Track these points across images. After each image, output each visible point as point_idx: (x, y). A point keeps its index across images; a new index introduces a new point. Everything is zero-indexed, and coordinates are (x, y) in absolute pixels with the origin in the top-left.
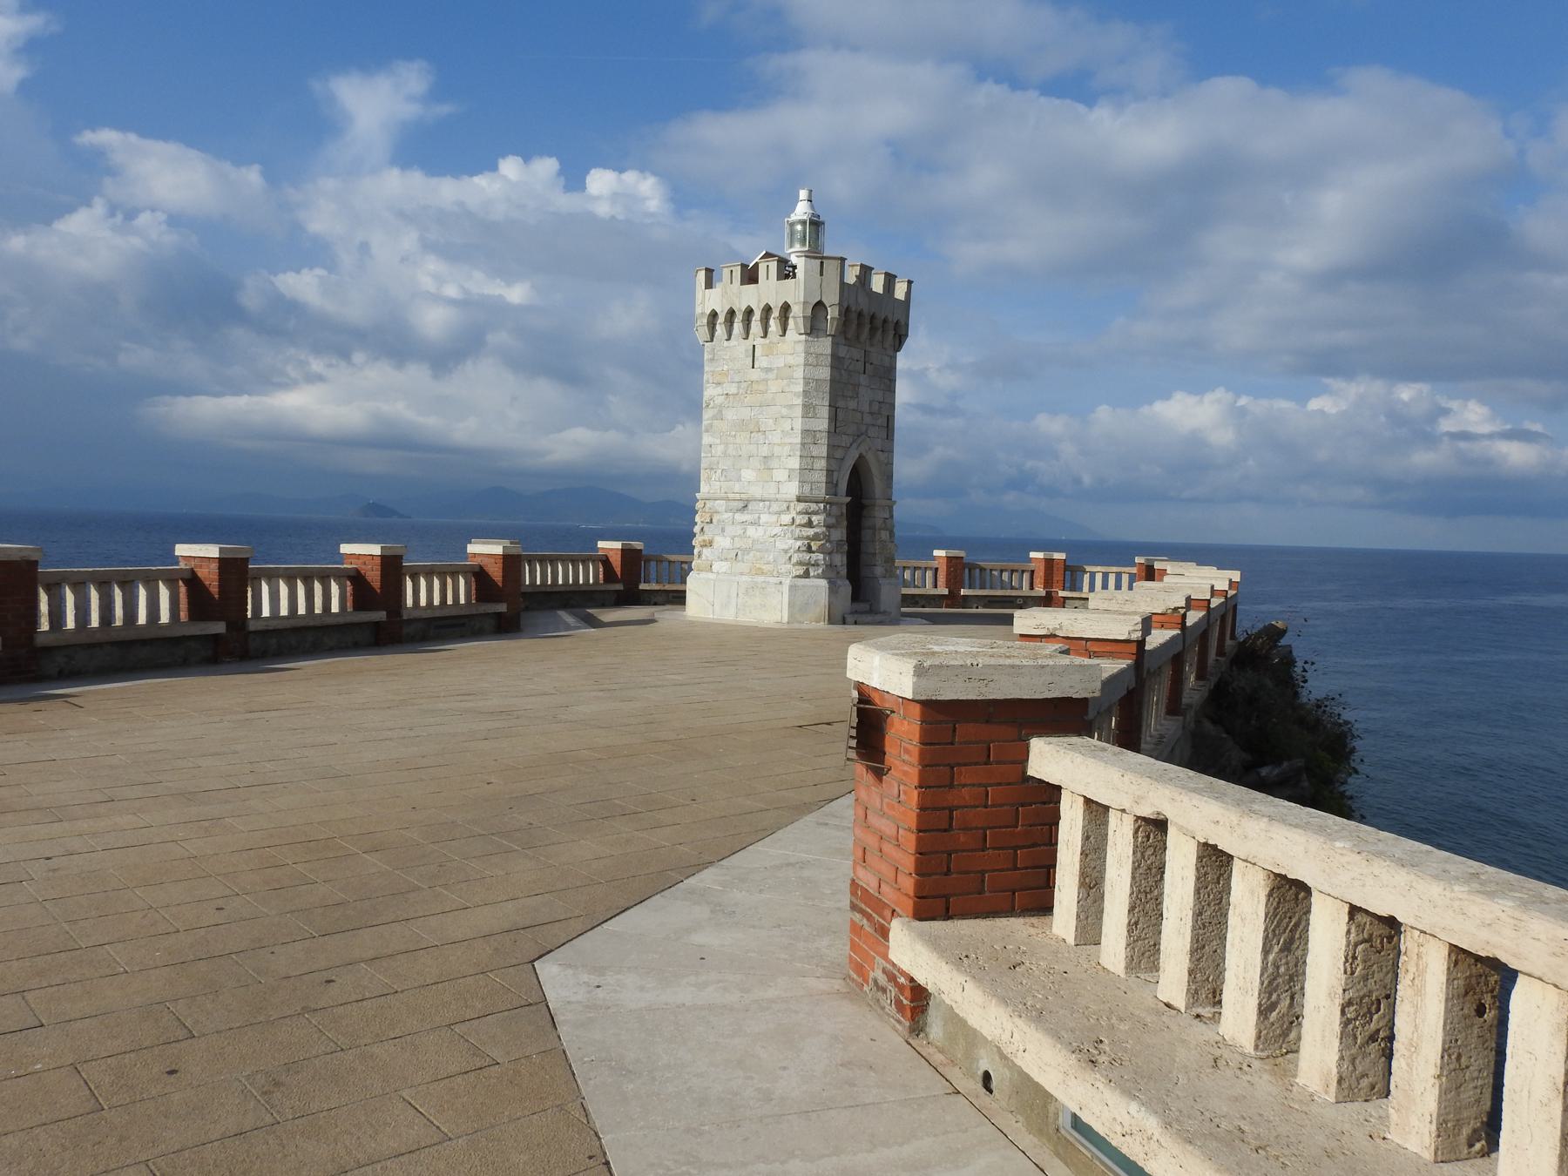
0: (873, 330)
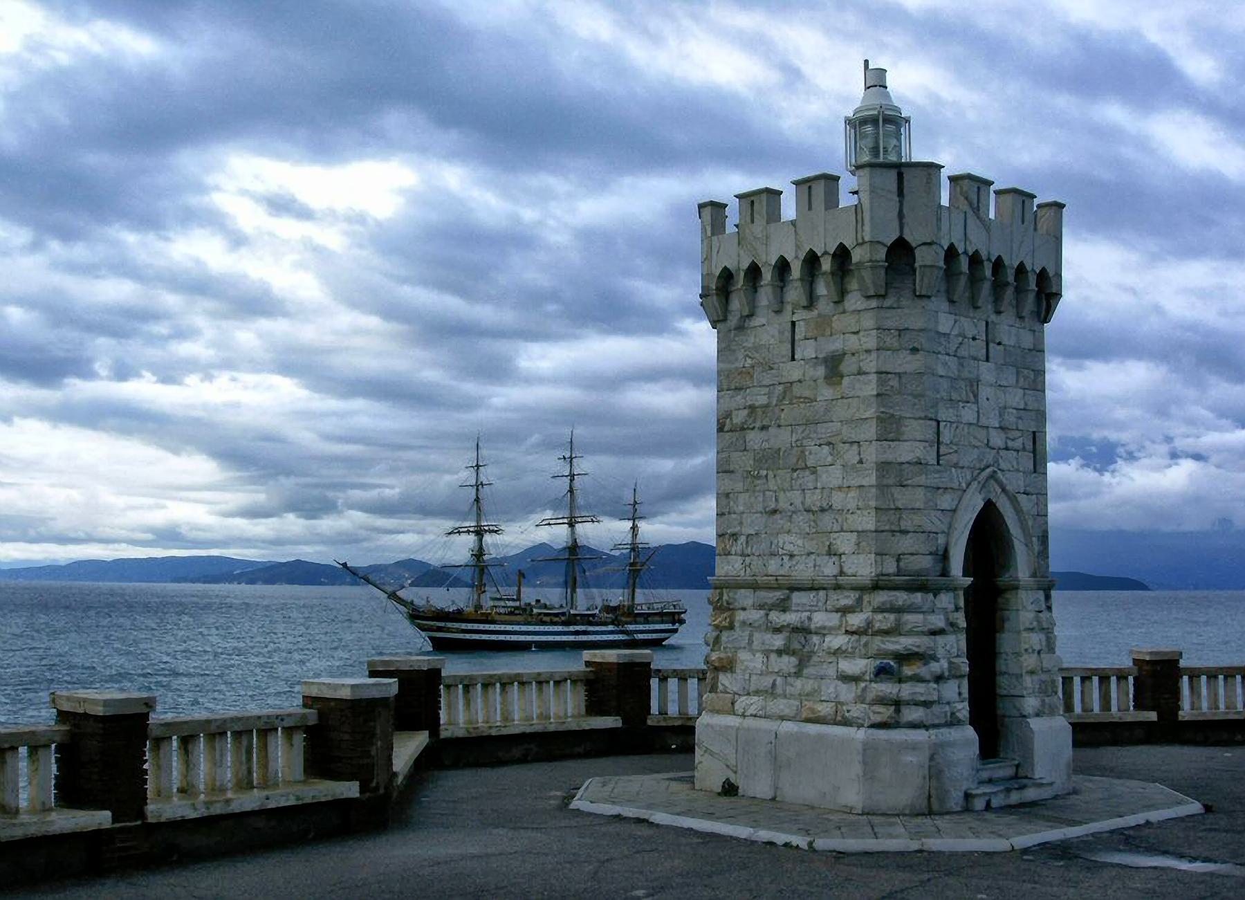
0: (998, 287)
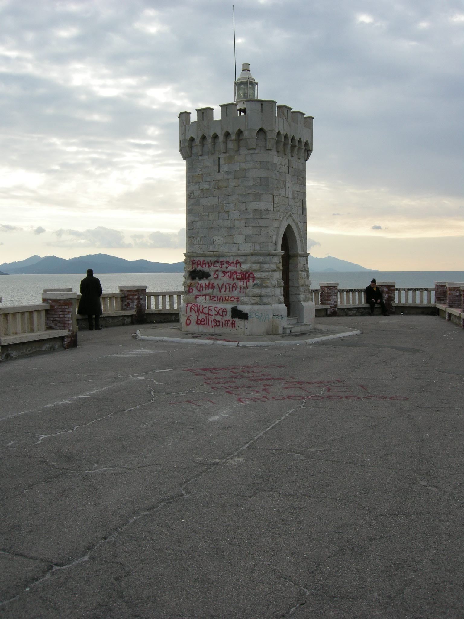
0: (293, 147)
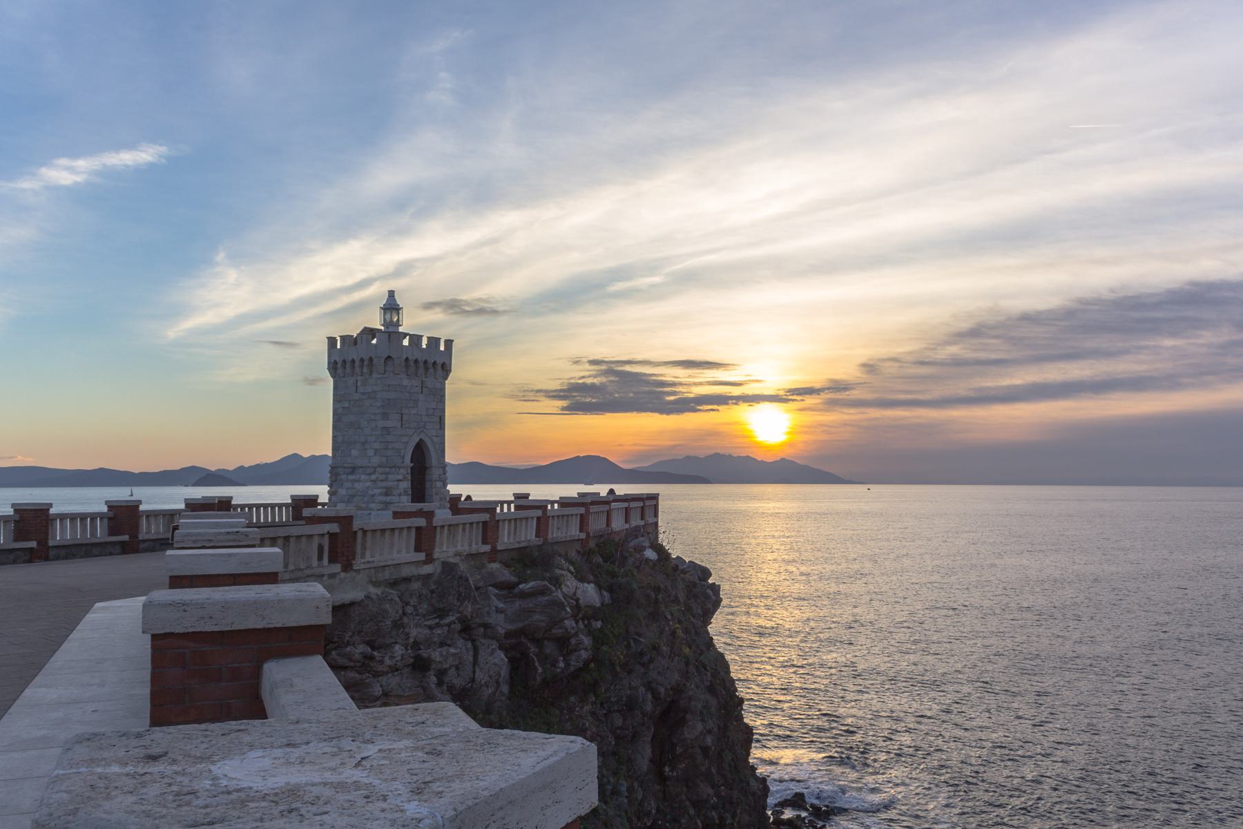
0: (427, 369)
